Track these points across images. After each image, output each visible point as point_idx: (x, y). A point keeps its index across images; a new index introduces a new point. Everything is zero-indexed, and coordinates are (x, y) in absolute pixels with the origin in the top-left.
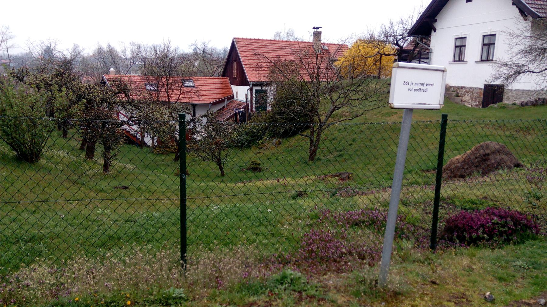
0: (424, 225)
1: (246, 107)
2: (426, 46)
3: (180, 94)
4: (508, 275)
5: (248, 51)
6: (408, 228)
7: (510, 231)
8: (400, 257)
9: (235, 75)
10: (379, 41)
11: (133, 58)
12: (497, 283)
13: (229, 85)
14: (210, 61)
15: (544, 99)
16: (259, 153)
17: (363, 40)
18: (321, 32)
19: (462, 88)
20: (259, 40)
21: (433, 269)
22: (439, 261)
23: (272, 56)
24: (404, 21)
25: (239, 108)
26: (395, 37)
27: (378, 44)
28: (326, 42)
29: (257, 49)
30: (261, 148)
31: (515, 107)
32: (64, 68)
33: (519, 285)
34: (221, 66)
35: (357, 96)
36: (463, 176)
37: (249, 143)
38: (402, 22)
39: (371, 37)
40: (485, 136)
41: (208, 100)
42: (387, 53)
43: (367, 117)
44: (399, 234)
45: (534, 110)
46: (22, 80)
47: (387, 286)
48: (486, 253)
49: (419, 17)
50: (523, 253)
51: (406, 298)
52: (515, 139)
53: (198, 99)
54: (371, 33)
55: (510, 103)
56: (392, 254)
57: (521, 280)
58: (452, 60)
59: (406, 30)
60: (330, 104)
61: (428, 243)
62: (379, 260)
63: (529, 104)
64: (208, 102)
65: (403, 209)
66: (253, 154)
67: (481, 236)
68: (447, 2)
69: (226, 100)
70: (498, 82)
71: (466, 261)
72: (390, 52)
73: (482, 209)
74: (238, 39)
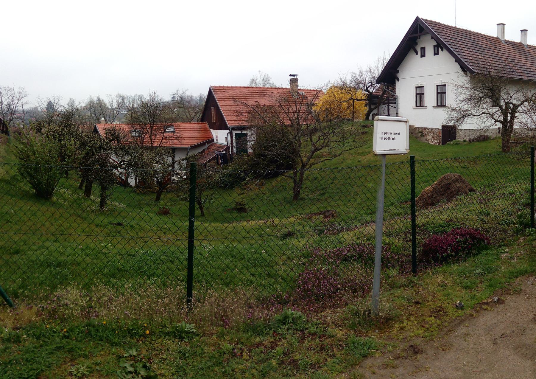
0: (406, 253)
1: (227, 149)
2: (392, 93)
3: (163, 139)
4: (471, 283)
5: (226, 97)
6: (393, 257)
7: (470, 246)
8: (388, 285)
9: (214, 120)
10: (351, 87)
11: (118, 108)
12: (464, 291)
13: (209, 129)
14: (188, 108)
15: (484, 136)
16: (243, 193)
17: (336, 87)
18: (297, 79)
19: (425, 128)
20: (236, 87)
21: (415, 291)
22: (420, 282)
23: (251, 102)
24: (372, 70)
25: (220, 150)
26: (364, 84)
27: (350, 90)
28: (302, 88)
29: (235, 95)
30: (245, 189)
31: (465, 143)
32: (66, 120)
33: (479, 289)
34: (199, 112)
35: (335, 138)
36: (433, 204)
37: (232, 184)
38: (370, 71)
39: (344, 85)
40: (446, 168)
41: (187, 143)
42: (359, 98)
43: (345, 157)
44: (386, 263)
45: (478, 145)
46: (40, 132)
47: (378, 314)
48: (455, 267)
49: (384, 68)
50: (480, 262)
51: (396, 322)
52: (468, 168)
53: (180, 143)
54: (343, 80)
55: (462, 140)
56: (381, 283)
57: (480, 285)
58: (415, 105)
59: (373, 77)
60: (311, 146)
61: (410, 268)
62: (371, 291)
63: (475, 140)
64: (187, 146)
65: (387, 240)
66: (237, 195)
67: (450, 254)
68: (404, 58)
69: (206, 143)
70: (451, 124)
71: (440, 278)
72: (361, 97)
73: (449, 230)
74: (215, 87)
